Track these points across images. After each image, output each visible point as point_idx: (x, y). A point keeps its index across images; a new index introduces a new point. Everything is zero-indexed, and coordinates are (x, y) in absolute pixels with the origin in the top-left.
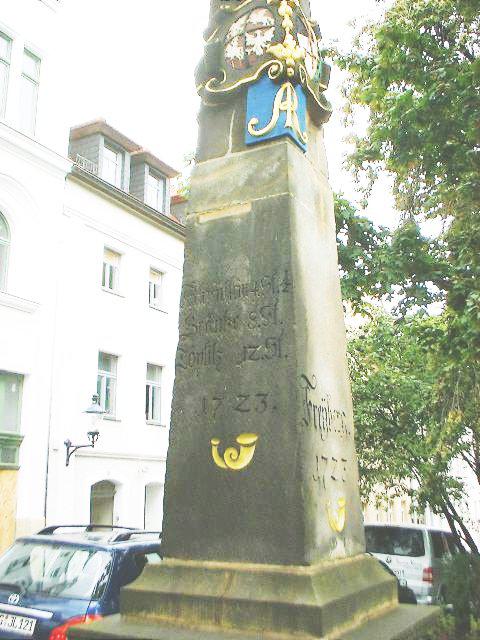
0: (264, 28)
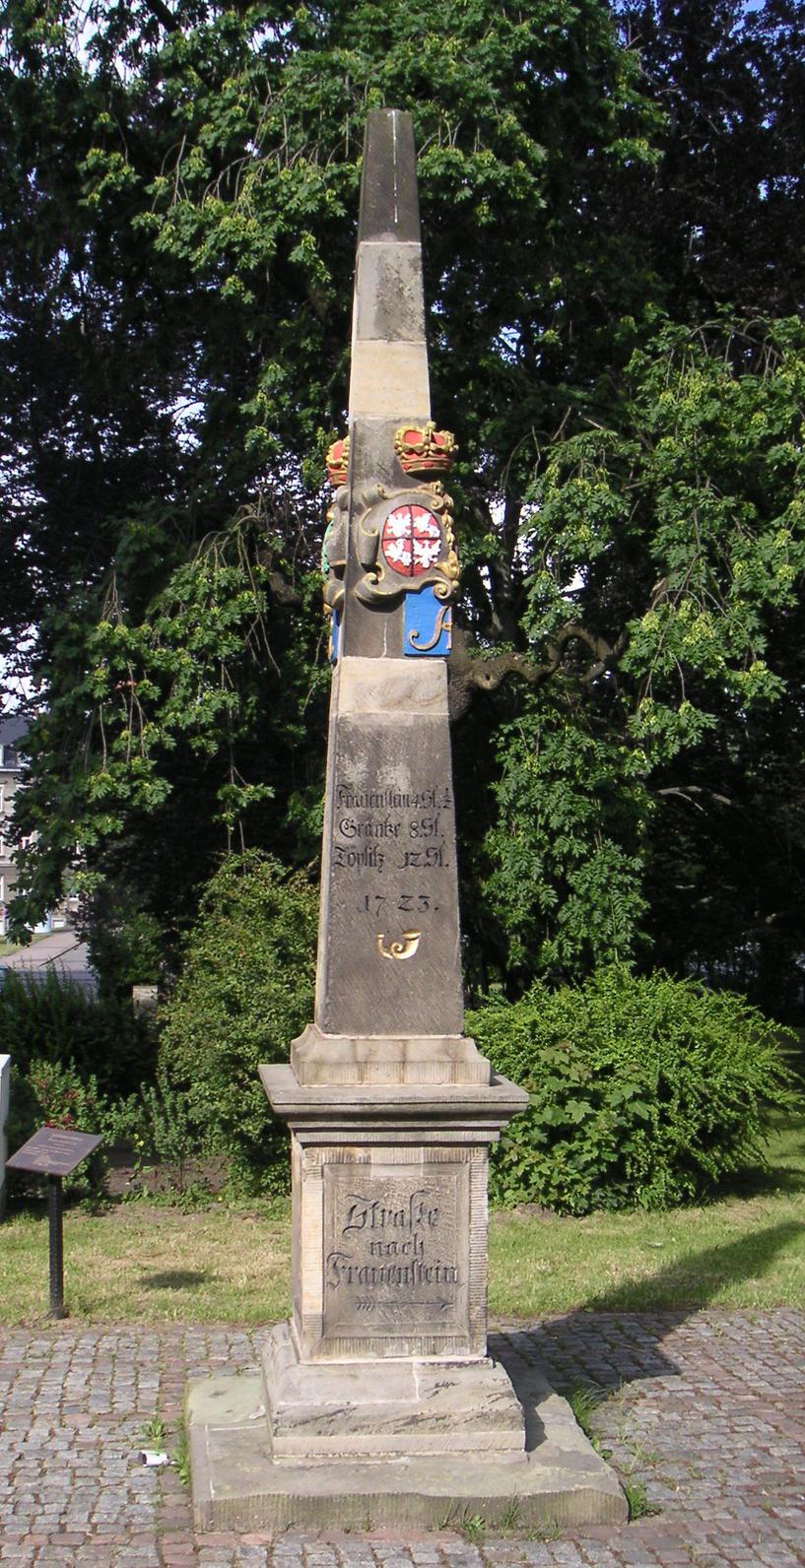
0: (434, 539)
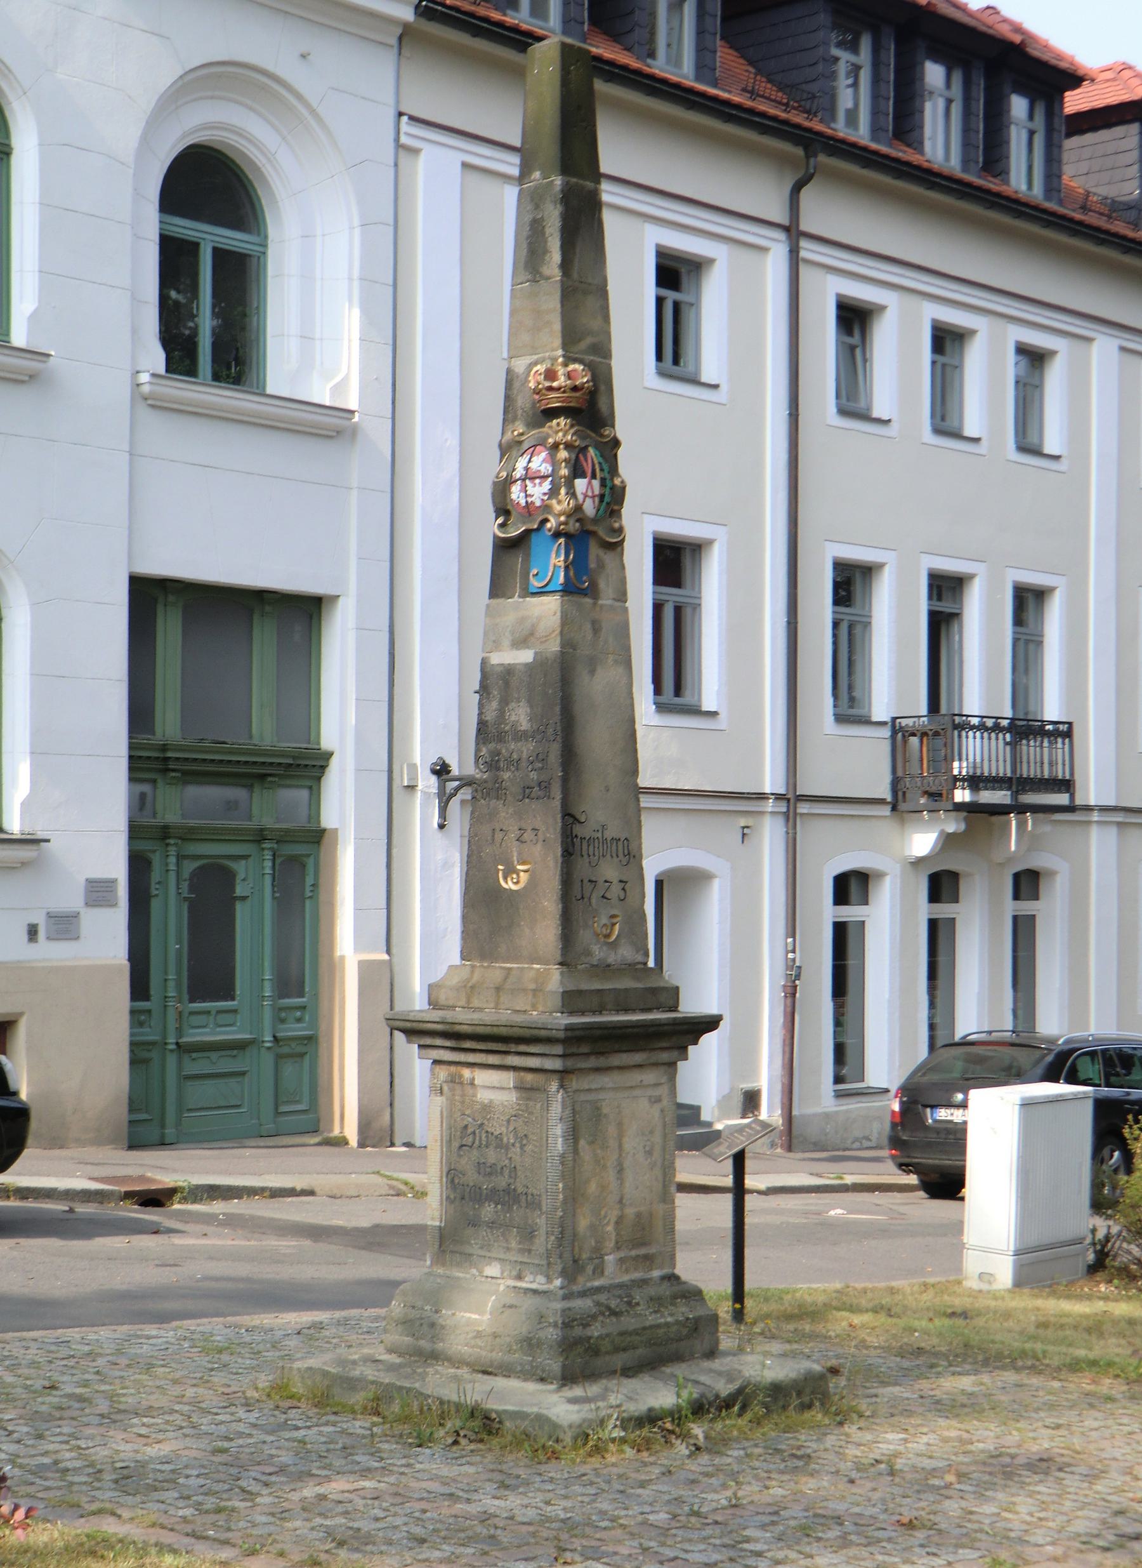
0: (545, 477)
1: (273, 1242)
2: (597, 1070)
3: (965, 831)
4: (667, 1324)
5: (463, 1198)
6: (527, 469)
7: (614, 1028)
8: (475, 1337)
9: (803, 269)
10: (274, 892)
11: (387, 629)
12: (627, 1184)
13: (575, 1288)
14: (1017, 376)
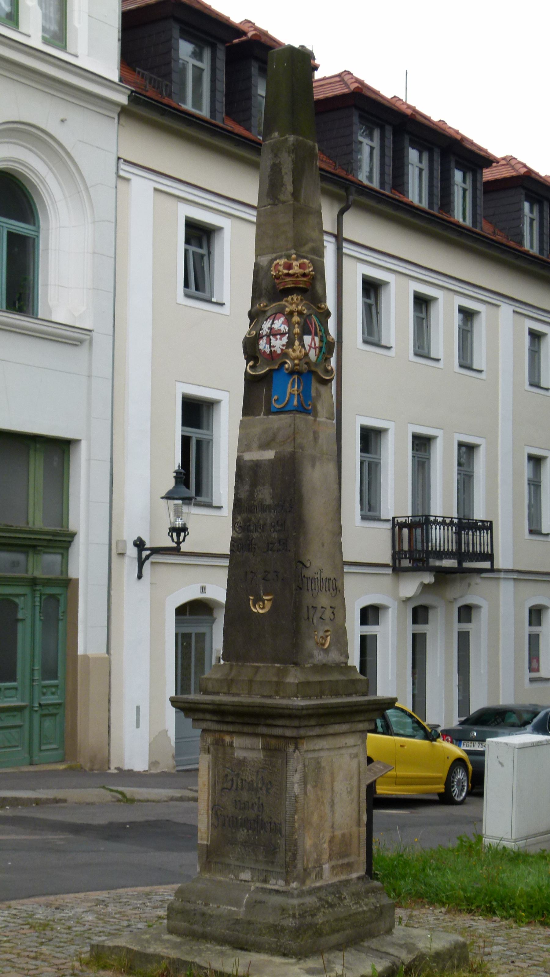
0: (283, 334)
1: (50, 836)
2: (319, 736)
3: (434, 583)
4: (364, 912)
5: (224, 825)
6: (271, 329)
7: (332, 708)
8: (235, 924)
9: (345, 260)
10: (40, 616)
11: (109, 460)
12: (336, 815)
13: (305, 888)
14: (459, 325)
